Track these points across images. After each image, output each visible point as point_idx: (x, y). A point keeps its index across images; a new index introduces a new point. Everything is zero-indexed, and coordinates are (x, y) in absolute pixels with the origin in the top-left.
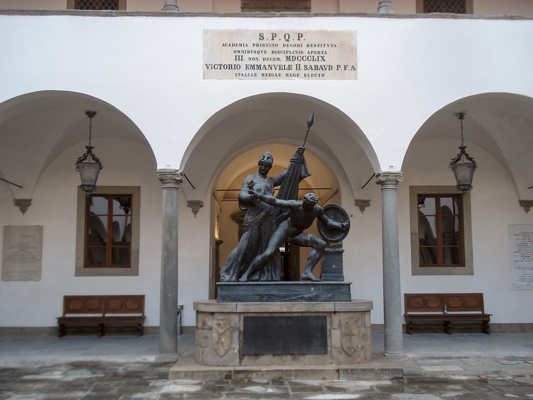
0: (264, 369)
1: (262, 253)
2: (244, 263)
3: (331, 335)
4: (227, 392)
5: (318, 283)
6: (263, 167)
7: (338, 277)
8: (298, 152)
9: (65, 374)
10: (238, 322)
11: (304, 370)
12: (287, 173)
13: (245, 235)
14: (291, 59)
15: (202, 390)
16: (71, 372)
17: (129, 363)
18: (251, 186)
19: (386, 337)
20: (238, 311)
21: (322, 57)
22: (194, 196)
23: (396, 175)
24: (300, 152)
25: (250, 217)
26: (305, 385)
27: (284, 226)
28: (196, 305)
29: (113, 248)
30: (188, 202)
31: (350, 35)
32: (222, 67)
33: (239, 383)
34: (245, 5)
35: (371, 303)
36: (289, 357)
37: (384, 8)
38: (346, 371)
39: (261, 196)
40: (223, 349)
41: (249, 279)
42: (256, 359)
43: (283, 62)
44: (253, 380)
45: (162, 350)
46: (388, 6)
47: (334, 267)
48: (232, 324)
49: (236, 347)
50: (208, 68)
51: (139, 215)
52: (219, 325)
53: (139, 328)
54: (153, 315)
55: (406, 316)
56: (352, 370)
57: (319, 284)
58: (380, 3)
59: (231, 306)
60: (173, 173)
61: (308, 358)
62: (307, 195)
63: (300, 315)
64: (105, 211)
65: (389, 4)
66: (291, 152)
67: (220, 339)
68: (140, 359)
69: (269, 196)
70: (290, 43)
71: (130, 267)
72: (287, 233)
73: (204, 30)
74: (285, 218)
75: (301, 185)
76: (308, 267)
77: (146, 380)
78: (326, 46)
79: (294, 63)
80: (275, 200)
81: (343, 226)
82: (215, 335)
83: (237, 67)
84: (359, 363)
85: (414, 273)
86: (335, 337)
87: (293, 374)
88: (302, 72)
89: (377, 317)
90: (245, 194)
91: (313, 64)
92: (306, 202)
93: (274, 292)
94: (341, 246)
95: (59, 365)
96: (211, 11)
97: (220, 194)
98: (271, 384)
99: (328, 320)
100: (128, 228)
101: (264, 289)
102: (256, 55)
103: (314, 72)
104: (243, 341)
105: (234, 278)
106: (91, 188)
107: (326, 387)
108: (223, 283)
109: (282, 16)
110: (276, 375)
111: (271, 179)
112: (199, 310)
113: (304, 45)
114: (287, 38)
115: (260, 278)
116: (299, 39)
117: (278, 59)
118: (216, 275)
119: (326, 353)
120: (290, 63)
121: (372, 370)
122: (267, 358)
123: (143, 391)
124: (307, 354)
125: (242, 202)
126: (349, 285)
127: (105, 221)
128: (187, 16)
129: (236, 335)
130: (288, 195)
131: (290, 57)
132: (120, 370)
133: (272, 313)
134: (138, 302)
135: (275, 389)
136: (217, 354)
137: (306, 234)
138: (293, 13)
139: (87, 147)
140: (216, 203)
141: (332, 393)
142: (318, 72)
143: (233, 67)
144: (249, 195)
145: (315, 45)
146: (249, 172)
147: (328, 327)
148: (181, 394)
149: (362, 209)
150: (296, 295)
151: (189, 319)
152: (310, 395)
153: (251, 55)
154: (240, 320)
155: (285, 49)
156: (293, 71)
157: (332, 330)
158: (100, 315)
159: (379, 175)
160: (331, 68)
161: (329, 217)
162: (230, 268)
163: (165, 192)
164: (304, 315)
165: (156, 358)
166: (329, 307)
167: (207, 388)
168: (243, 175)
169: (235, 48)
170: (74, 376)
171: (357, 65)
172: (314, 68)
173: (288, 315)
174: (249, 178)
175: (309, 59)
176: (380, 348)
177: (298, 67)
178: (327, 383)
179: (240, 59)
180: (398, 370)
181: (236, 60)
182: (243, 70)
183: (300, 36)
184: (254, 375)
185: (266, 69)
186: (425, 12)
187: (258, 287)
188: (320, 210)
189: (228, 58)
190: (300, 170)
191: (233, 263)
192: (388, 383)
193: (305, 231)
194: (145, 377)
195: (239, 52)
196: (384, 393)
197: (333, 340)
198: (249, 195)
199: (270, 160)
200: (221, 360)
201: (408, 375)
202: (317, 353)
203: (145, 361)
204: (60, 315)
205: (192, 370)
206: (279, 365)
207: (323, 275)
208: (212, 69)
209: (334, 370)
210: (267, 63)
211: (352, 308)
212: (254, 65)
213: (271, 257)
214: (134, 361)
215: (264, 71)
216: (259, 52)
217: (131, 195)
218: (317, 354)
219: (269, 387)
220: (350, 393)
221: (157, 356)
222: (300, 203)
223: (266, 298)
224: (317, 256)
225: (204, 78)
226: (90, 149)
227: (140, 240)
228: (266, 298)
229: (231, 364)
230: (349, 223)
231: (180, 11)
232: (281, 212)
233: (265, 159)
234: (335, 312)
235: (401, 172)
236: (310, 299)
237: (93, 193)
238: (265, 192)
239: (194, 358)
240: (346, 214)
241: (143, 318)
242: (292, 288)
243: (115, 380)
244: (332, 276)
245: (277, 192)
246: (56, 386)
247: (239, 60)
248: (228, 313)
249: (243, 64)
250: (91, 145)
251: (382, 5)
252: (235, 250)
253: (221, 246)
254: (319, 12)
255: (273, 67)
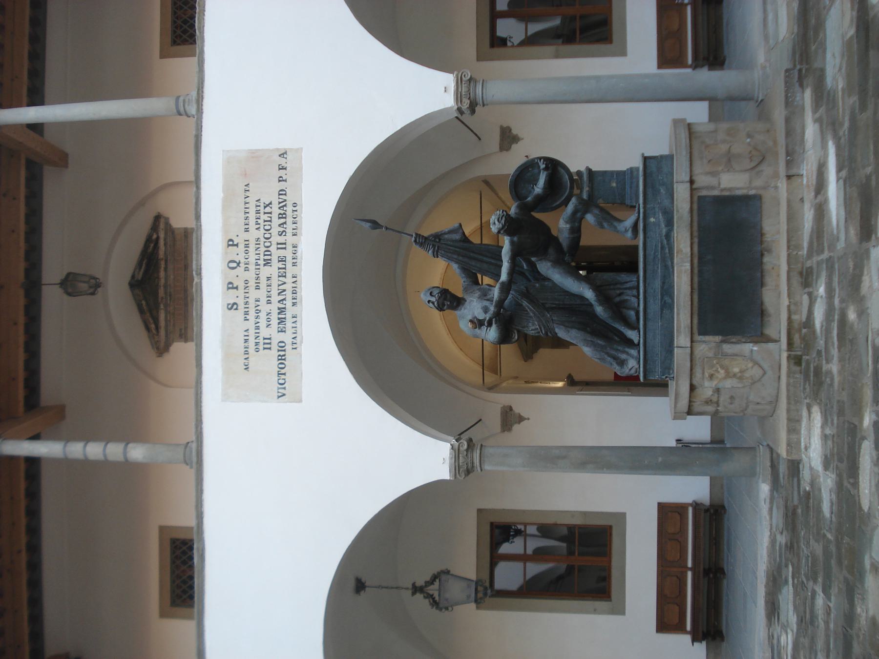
0: (785, 301)
1: (591, 305)
2: (607, 336)
3: (730, 189)
4: (824, 362)
5: (642, 210)
6: (446, 303)
7: (632, 177)
8: (421, 245)
9: (785, 628)
10: (707, 346)
11: (788, 235)
12: (456, 263)
13: (561, 333)
14: (269, 257)
15: (819, 404)
16: (783, 618)
17: (771, 525)
18: (478, 323)
19: (732, 99)
20: (689, 345)
21: (265, 207)
22: (494, 420)
23: (459, 82)
24: (422, 241)
25: (530, 324)
26: (812, 232)
27: (545, 268)
28: (677, 416)
29: (579, 555)
30: (503, 431)
31: (229, 161)
32: (283, 371)
33: (808, 342)
34: (181, 336)
35: (676, 123)
36: (766, 259)
37: (186, 106)
38: (789, 164)
39: (496, 306)
40: (751, 369)
41: (635, 327)
42: (769, 316)
43: (273, 270)
44: (804, 319)
45: (752, 474)
46: (184, 101)
47: (614, 185)
48: (711, 355)
49: (748, 348)
50: (284, 395)
51: (524, 511)
52: (711, 377)
53: (712, 511)
54: (692, 489)
55: (696, 66)
56: (788, 154)
57: (644, 208)
58: (180, 114)
59: (680, 356)
60: (456, 453)
61: (768, 226)
62: (494, 229)
63: (696, 240)
64: (518, 566)
65: (181, 99)
66: (421, 256)
67: (735, 375)
68: (764, 508)
69: (496, 293)
70: (243, 261)
71: (611, 527)
72: (559, 262)
73: (223, 401)
74: (533, 266)
75: (476, 240)
76: (615, 227)
77: (800, 498)
78: (247, 200)
79: (276, 254)
80: (503, 283)
81: (546, 169)
82: (729, 383)
83: (282, 348)
84: (775, 142)
85: (623, 53)
86: (733, 182)
87: (795, 253)
88: (289, 239)
89: (697, 113)
90: (492, 333)
91: (276, 222)
92: (505, 231)
93: (657, 284)
94: (579, 173)
95: (771, 637)
96: (193, 391)
97: (490, 378)
98: (811, 290)
99: (704, 193)
100: (545, 530)
101: (652, 301)
102: (263, 315)
103: (289, 220)
104: (739, 337)
105: (633, 352)
106: (480, 588)
107: (816, 196)
108: (642, 369)
109: (199, 274)
110: (796, 280)
111: (466, 290)
112: (686, 410)
113: (246, 236)
114: (235, 265)
115: (633, 309)
116: (237, 245)
117: (269, 279)
118: (626, 383)
119: (758, 198)
120: (275, 259)
121: (788, 120)
122: (768, 297)
123: (820, 501)
124: (761, 228)
125: (505, 338)
126: (646, 159)
127: (534, 569)
128: (201, 428)
129: (727, 348)
130: (493, 261)
131: (265, 260)
132: (782, 539)
133: (692, 288)
134: (669, 513)
135: (819, 282)
136: (760, 380)
137: (560, 230)
138: (194, 256)
139: (414, 594)
140: (504, 384)
141: (827, 186)
142: (289, 213)
143: (282, 353)
144: (494, 326)
145: (247, 218)
146: (453, 330)
147: (716, 193)
148: (825, 437)
149: (515, 139)
150: (663, 248)
151: (698, 429)
152: (830, 222)
153: (263, 323)
154: (704, 342)
155: (252, 267)
156: (288, 254)
157: (722, 186)
158: (690, 574)
159: (459, 110)
160: (282, 192)
161: (530, 192)
162: (615, 358)
163: (487, 467)
164: (696, 234)
165: (763, 482)
166: (682, 193)
167: (815, 395)
168: (462, 335)
169: (252, 350)
170: (789, 614)
171: (278, 149)
172: (283, 221)
173: (696, 261)
174: (465, 326)
175: (267, 227)
176: (750, 108)
177: (282, 246)
178: (809, 195)
179: (268, 341)
180: (786, 77)
181: (270, 349)
182: (287, 337)
183: (231, 243)
184: (795, 317)
185: (284, 299)
186: (194, 42)
187: (648, 311)
188: (518, 207)
189: (267, 361)
190: (452, 241)
191: (608, 354)
192: (808, 94)
193: (554, 232)
194: (796, 502)
195: (257, 344)
196: (825, 100)
197: (739, 186)
198: (494, 326)
199: (436, 292)
200: (769, 373)
201: (795, 61)
202: (759, 212)
203: (768, 501)
204: (688, 638)
205: (785, 421)
206: (778, 276)
207: (628, 202)
208: (284, 388)
209: (788, 184)
210: (275, 298)
211: (684, 153)
212: (279, 319)
213: (598, 290)
214: (768, 518)
215: (289, 303)
216: (258, 311)
217: (492, 524)
218: (761, 212)
219: (815, 293)
220: (826, 156)
221: (760, 481)
222: (506, 243)
223: (666, 298)
224: (596, 211)
225: (300, 401)
226: (416, 589)
227: (566, 509)
228: (666, 298)
229: (778, 358)
230: (540, 158)
231: (194, 438)
232: (522, 274)
233: (433, 299)
234: (692, 182)
235: (455, 73)
236: (670, 223)
237: (487, 584)
238: (488, 300)
239: (765, 419)
240: (525, 163)
241: (696, 505)
242: (651, 253)
243: (799, 547)
244: (631, 188)
245: (487, 280)
246: (806, 641)
247: (270, 344)
248: (691, 361)
249: (277, 337)
250: (410, 586)
251: (182, 109)
252: (585, 351)
253: (577, 378)
254: (194, 212)
255: (282, 287)
